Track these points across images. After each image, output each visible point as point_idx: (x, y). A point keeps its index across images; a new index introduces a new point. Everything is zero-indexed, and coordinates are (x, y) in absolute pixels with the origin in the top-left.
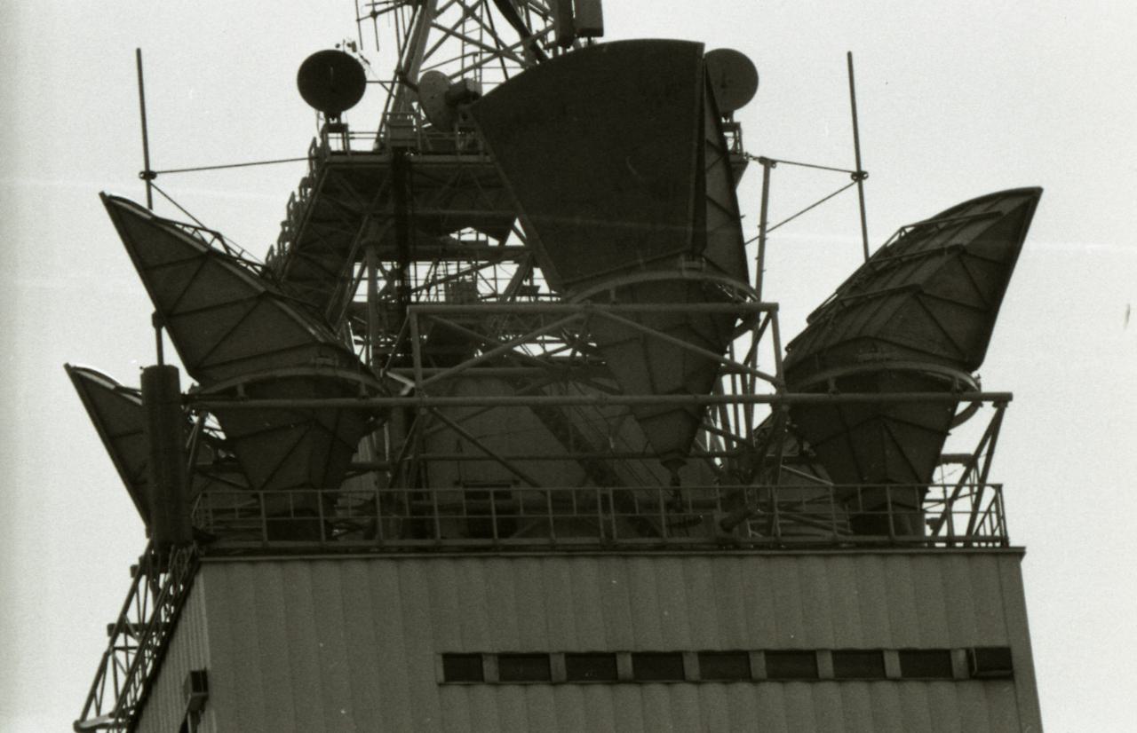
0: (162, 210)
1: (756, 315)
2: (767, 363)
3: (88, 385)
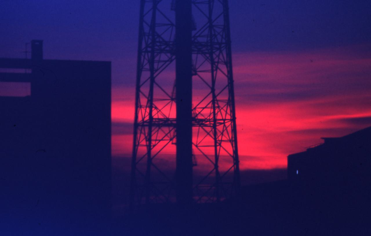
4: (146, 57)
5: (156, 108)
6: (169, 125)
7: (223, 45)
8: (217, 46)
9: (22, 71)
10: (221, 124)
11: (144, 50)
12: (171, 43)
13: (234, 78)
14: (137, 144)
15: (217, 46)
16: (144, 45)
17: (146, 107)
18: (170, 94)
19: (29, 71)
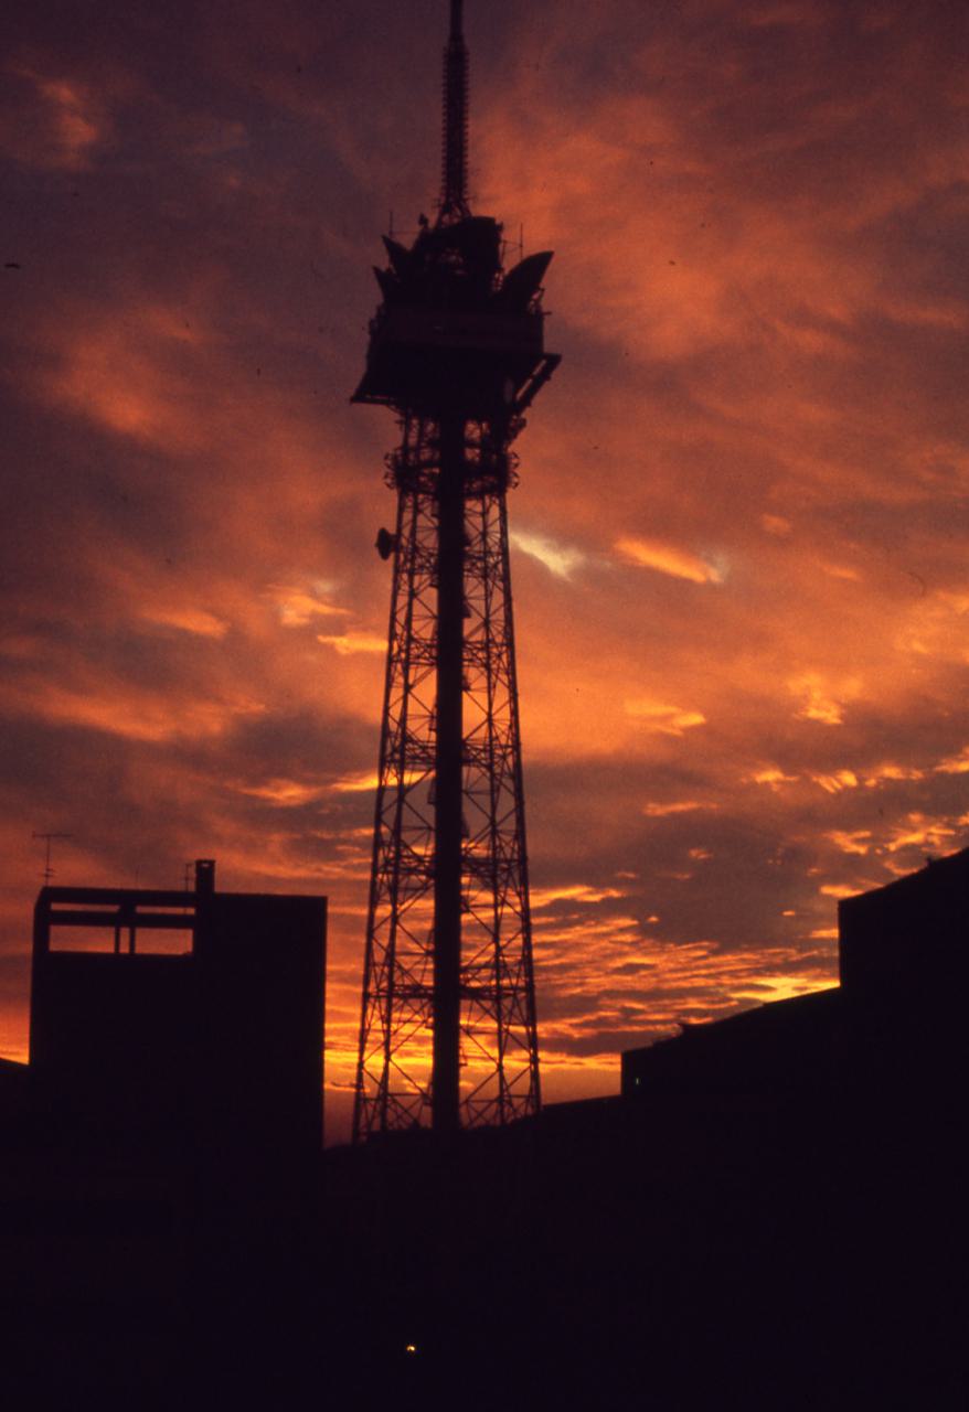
0: (394, 239)
1: (501, 270)
2: (501, 278)
3: (377, 271)
4: (376, 1012)
5: (400, 967)
6: (421, 996)
7: (509, 750)
8: (505, 866)
9: (179, 911)
10: (509, 995)
11: (389, 759)
12: (430, 745)
13: (523, 738)
14: (367, 1027)
15: (505, 866)
16: (389, 750)
17: (384, 965)
18: (430, 708)
19: (191, 911)
